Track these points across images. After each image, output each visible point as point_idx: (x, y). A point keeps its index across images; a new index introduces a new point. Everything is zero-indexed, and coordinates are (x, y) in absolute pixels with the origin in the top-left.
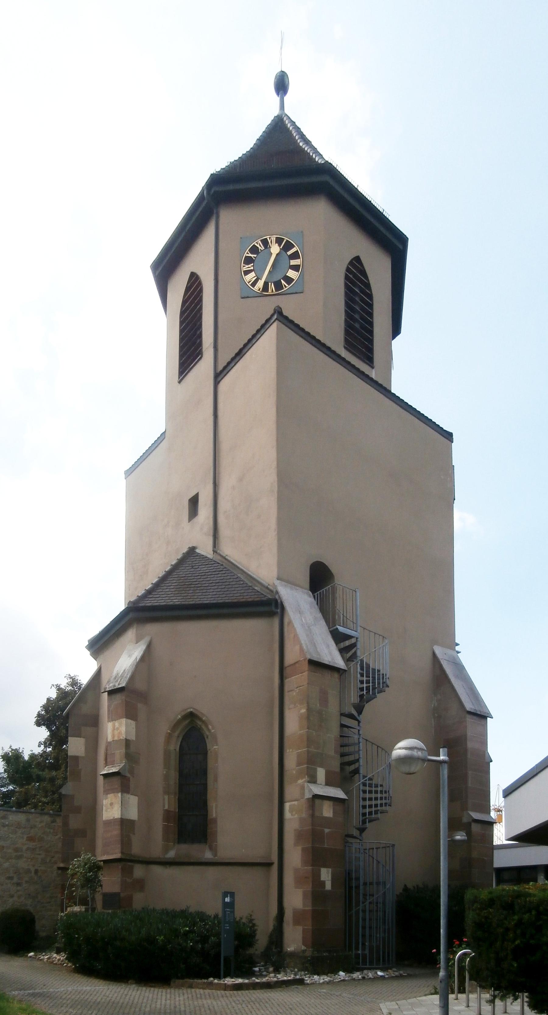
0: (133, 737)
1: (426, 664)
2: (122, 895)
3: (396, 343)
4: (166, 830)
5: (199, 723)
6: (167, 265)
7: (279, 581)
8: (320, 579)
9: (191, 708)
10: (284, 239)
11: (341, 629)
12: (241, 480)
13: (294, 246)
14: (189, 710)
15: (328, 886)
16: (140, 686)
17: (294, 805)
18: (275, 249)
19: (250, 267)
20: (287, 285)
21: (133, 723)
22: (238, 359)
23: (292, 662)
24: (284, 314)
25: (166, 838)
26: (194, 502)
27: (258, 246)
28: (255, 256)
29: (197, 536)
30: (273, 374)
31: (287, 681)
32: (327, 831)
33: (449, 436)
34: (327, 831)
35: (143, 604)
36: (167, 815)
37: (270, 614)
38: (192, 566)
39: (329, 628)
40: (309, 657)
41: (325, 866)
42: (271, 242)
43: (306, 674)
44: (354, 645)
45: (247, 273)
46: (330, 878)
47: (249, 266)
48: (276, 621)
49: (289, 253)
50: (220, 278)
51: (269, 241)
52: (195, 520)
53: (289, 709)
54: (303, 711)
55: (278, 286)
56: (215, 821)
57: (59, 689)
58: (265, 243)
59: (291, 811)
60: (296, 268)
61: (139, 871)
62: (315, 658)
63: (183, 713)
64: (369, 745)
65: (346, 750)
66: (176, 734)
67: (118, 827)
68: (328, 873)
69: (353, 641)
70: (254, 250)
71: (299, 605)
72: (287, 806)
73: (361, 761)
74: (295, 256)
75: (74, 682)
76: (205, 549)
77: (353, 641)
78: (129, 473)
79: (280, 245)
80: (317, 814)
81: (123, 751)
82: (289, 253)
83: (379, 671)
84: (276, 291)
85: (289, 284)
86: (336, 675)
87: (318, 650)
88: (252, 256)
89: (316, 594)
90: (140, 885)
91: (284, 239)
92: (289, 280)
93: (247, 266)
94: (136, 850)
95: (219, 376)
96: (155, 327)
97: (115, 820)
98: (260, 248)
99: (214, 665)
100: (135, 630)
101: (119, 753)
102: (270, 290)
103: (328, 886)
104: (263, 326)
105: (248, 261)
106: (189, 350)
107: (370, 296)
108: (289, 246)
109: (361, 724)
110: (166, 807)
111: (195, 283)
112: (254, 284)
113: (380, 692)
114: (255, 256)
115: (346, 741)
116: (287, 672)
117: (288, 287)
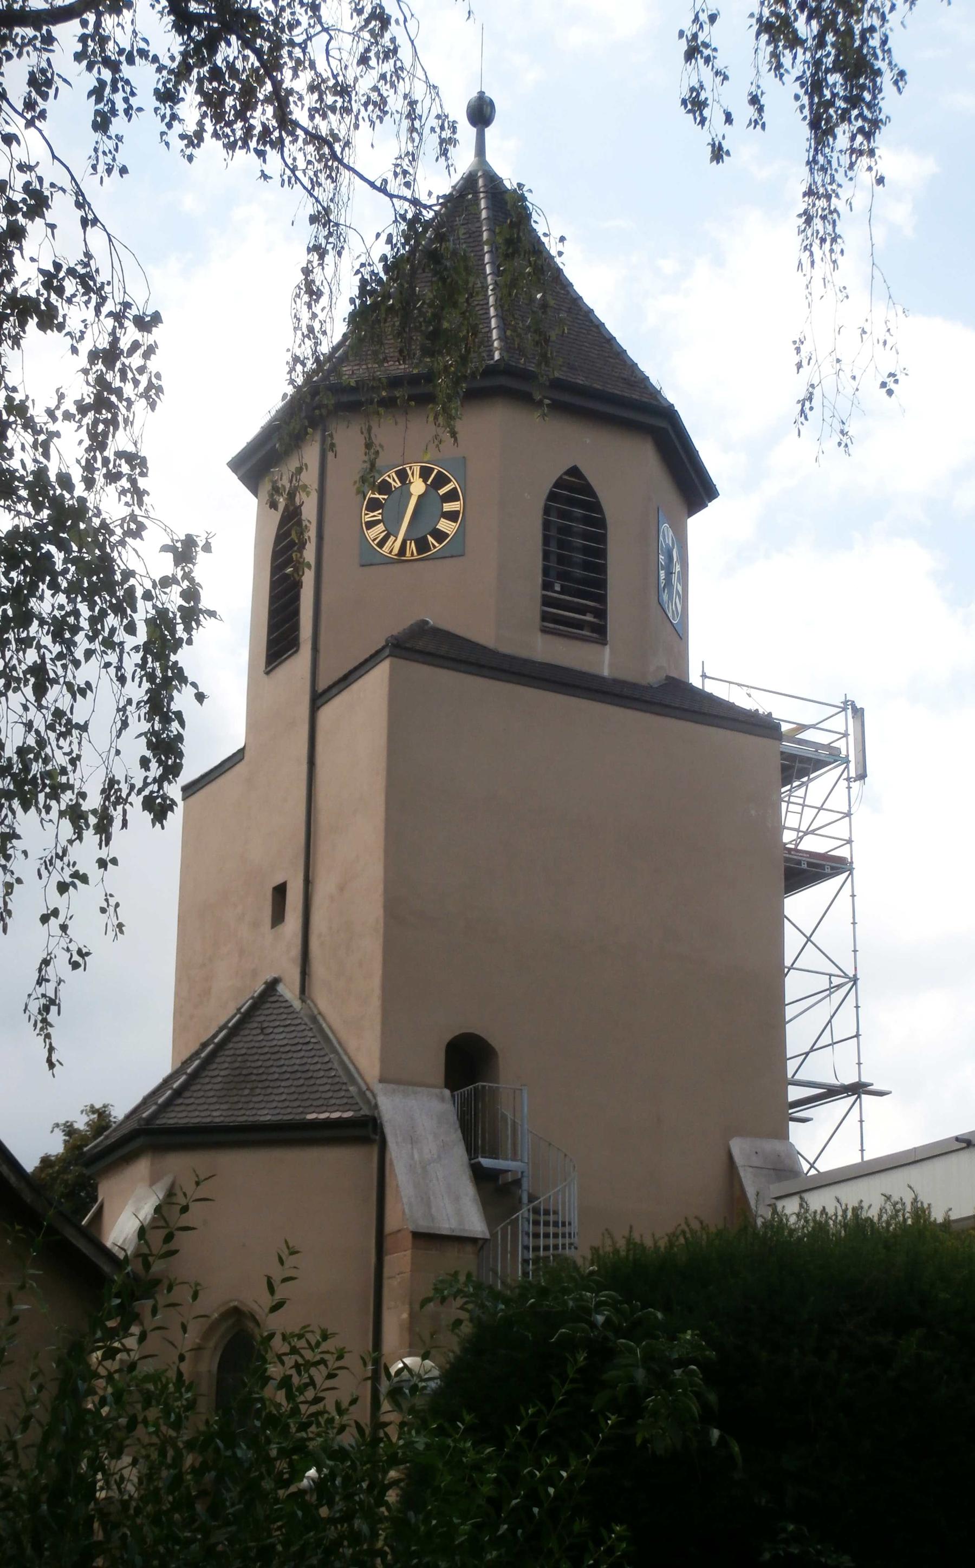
5: (251, 1325)
7: (381, 1085)
8: (467, 1064)
9: (235, 1300)
10: (433, 469)
12: (342, 888)
13: (450, 481)
14: (232, 1304)
18: (418, 487)
19: (377, 515)
20: (436, 544)
22: (342, 686)
23: (395, 1228)
26: (280, 891)
27: (391, 481)
28: (386, 497)
30: (381, 740)
31: (388, 1259)
35: (164, 1121)
37: (364, 1140)
38: (262, 1029)
39: (470, 1159)
40: (411, 1228)
42: (413, 474)
43: (409, 1252)
45: (370, 525)
47: (375, 513)
49: (442, 492)
51: (410, 473)
52: (280, 928)
53: (388, 1309)
54: (405, 1316)
55: (422, 546)
57: (69, 1130)
58: (402, 475)
60: (452, 516)
62: (424, 1226)
63: (222, 1309)
66: (211, 1344)
71: (420, 1124)
74: (452, 496)
75: (101, 1117)
79: (425, 481)
82: (442, 492)
84: (419, 554)
85: (440, 543)
86: (469, 1248)
87: (433, 1210)
88: (381, 497)
89: (456, 1093)
91: (433, 469)
92: (440, 536)
93: (372, 514)
98: (393, 483)
100: (149, 1163)
102: (408, 554)
104: (372, 657)
105: (374, 505)
108: (442, 480)
112: (381, 544)
114: (386, 497)
116: (388, 1244)
117: (439, 546)
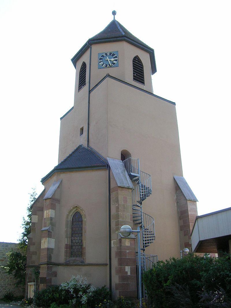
0: (53, 216)
1: (171, 181)
2: (47, 278)
3: (154, 77)
4: (66, 252)
6: (75, 60)
11: (132, 174)
14: (75, 205)
15: (129, 274)
16: (57, 197)
17: (115, 241)
19: (101, 60)
21: (54, 211)
24: (110, 75)
25: (66, 256)
26: (82, 129)
29: (82, 141)
32: (127, 251)
33: (174, 104)
34: (127, 251)
36: (67, 246)
41: (127, 265)
44: (138, 179)
45: (100, 62)
46: (130, 270)
48: (108, 171)
50: (91, 64)
56: (85, 248)
59: (114, 244)
61: (54, 269)
64: (147, 215)
65: (135, 219)
67: (46, 251)
68: (129, 268)
69: (137, 178)
70: (103, 56)
72: (112, 242)
73: (143, 222)
76: (85, 145)
77: (137, 178)
78: (61, 119)
80: (123, 245)
81: (49, 222)
83: (148, 188)
90: (55, 274)
94: (53, 260)
95: (90, 92)
96: (71, 74)
97: (45, 248)
99: (86, 187)
101: (48, 222)
103: (129, 274)
105: (100, 59)
106: (82, 81)
107: (142, 65)
109: (142, 209)
110: (66, 243)
111: (84, 65)
112: (102, 65)
113: (147, 196)
115: (135, 215)
